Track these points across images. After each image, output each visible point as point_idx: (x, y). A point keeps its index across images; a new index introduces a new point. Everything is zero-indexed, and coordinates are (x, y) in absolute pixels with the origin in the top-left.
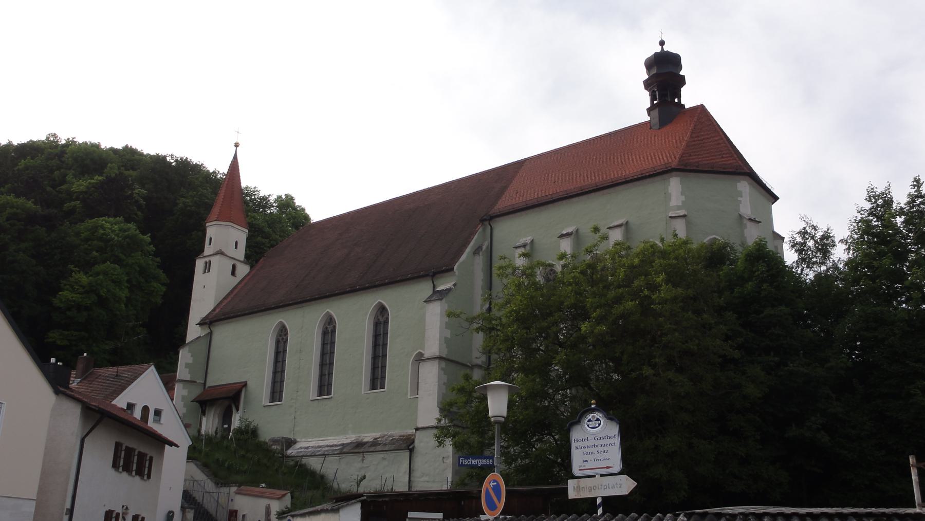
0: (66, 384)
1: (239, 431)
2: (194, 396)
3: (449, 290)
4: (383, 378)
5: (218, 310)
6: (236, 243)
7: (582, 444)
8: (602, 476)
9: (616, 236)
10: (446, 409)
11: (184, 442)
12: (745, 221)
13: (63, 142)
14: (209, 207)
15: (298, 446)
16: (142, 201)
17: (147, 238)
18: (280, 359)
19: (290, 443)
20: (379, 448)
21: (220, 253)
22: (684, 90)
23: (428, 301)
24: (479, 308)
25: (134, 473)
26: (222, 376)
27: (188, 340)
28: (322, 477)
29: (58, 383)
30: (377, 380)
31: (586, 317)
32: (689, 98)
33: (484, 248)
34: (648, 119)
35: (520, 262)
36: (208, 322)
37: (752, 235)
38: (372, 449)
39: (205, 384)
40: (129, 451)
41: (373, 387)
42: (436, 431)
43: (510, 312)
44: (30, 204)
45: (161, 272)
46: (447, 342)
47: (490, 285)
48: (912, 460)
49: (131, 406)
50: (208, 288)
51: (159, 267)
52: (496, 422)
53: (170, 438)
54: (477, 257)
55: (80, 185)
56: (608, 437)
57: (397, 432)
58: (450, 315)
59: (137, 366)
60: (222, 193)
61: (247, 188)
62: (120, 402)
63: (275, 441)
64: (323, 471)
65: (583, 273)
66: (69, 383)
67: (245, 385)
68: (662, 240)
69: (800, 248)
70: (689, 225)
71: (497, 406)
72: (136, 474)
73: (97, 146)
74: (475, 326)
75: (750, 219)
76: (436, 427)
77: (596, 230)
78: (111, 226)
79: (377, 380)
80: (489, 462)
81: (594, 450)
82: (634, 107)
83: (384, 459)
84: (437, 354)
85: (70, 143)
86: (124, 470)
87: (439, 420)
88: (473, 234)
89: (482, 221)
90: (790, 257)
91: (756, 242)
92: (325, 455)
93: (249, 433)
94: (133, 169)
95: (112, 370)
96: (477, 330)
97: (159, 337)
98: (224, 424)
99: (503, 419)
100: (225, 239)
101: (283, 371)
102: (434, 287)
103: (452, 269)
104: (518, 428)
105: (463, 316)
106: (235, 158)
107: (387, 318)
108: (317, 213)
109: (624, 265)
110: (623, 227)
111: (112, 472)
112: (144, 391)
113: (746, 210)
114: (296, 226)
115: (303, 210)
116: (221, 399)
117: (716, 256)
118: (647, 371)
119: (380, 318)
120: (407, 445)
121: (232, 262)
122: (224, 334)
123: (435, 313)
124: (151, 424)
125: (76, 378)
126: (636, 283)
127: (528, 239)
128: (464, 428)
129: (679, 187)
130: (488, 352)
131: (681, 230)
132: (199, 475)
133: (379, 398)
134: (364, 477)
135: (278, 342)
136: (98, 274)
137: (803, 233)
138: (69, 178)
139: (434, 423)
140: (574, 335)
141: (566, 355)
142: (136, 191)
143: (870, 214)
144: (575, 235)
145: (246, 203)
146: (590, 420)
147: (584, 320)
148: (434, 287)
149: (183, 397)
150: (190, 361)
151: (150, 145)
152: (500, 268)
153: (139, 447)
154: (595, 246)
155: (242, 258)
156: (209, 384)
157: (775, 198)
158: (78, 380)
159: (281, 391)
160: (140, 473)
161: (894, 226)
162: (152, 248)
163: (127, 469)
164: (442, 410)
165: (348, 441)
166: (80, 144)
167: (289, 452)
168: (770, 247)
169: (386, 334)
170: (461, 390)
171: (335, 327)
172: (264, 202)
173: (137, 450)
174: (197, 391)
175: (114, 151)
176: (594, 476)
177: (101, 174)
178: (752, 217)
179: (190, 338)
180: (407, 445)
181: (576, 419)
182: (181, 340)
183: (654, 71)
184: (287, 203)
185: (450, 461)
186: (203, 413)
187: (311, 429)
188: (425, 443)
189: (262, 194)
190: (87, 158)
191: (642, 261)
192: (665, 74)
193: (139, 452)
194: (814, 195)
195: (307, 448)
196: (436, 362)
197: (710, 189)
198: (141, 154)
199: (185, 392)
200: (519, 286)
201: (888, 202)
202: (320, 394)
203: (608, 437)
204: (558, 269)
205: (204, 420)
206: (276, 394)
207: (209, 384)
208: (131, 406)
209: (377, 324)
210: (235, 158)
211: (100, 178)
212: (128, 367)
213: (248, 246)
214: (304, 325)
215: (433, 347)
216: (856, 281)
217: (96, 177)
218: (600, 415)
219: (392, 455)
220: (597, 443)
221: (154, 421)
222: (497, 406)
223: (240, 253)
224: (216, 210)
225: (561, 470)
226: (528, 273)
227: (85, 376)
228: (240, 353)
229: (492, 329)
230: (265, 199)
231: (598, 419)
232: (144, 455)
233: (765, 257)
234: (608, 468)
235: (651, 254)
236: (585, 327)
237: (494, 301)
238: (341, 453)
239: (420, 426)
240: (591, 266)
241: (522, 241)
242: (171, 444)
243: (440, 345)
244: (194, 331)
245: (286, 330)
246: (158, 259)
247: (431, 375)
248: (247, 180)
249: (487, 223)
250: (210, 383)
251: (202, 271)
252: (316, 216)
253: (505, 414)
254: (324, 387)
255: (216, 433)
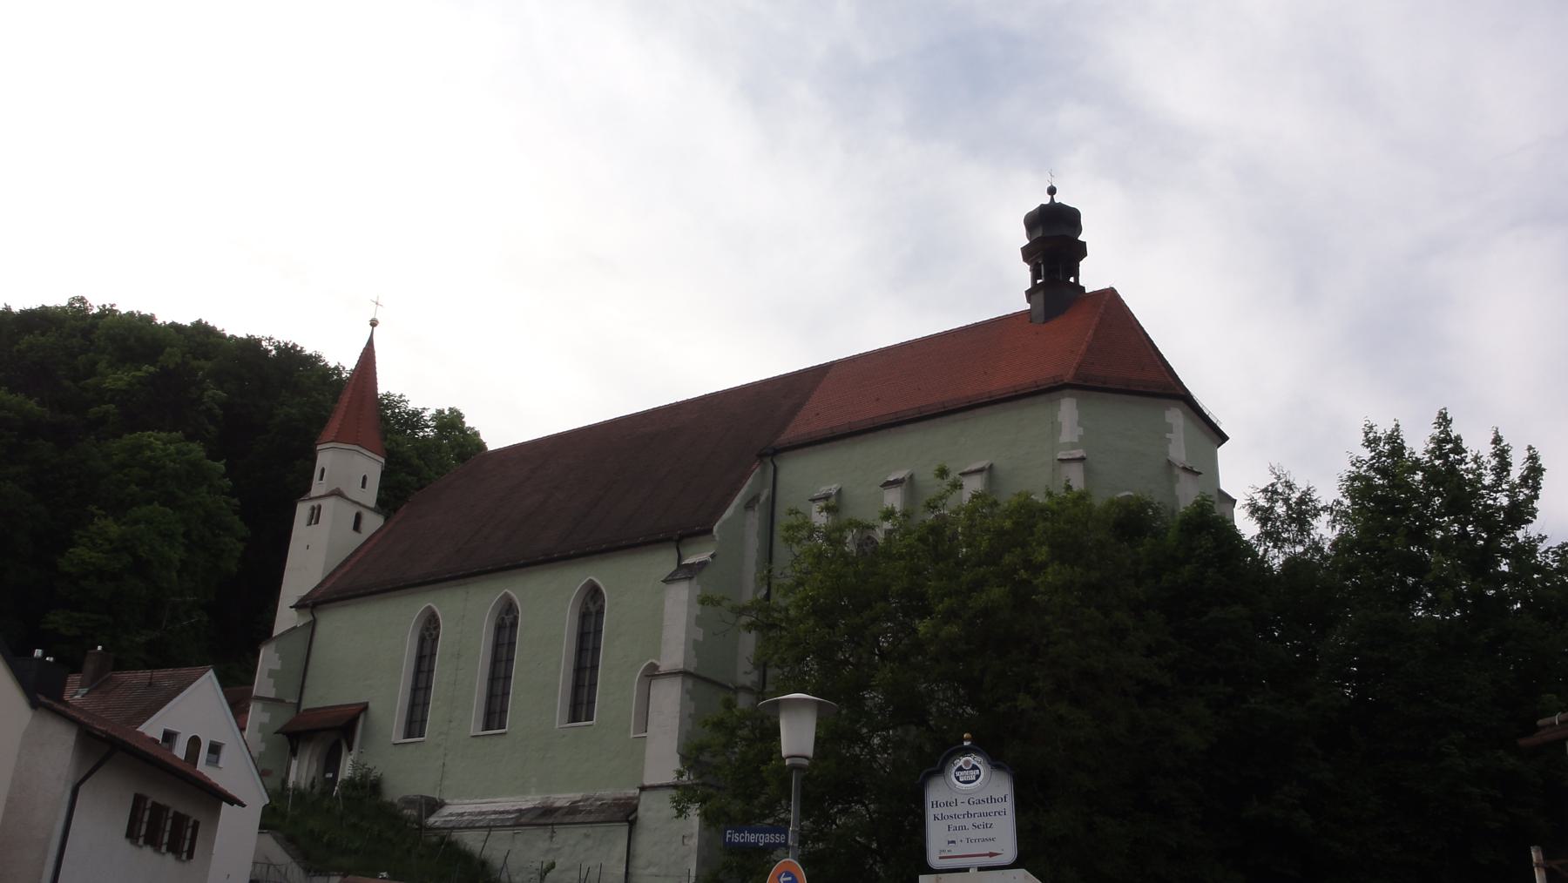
0: (58, 695)
1: (350, 783)
2: (278, 726)
3: (703, 564)
4: (591, 702)
5: (328, 585)
6: (365, 478)
7: (946, 811)
8: (980, 869)
9: (974, 485)
10: (691, 756)
11: (255, 797)
12: (1177, 471)
13: (96, 311)
14: (322, 422)
15: (446, 811)
16: (218, 411)
17: (220, 466)
18: (425, 667)
19: (434, 805)
20: (579, 818)
21: (337, 493)
22: (1084, 265)
23: (670, 580)
24: (750, 592)
25: (164, 849)
26: (328, 691)
27: (275, 633)
28: (484, 864)
29: (42, 692)
30: (581, 705)
31: (925, 612)
32: (1091, 276)
33: (763, 499)
34: (1028, 307)
35: (820, 519)
36: (311, 604)
37: (1187, 495)
38: (567, 820)
39: (299, 704)
40: (158, 810)
41: (574, 717)
42: (674, 792)
43: (804, 599)
44: (32, 405)
45: (237, 518)
46: (696, 647)
47: (769, 554)
48: (1536, 855)
49: (169, 736)
50: (314, 549)
51: (235, 513)
52: (794, 767)
53: (231, 791)
54: (751, 513)
55: (118, 379)
56: (992, 800)
57: (609, 793)
58: (704, 601)
59: (184, 671)
60: (345, 398)
61: (388, 395)
62: (153, 728)
63: (409, 802)
64: (486, 853)
65: (921, 539)
66: (62, 692)
67: (364, 708)
68: (1049, 494)
69: (1262, 515)
70: (1088, 473)
71: (797, 736)
72: (168, 850)
73: (149, 319)
74: (745, 620)
75: (1185, 469)
76: (675, 786)
77: (943, 473)
78: (159, 442)
79: (581, 705)
80: (778, 838)
81: (968, 822)
82: (1008, 288)
83: (587, 836)
84: (681, 667)
85: (107, 314)
86: (146, 843)
87: (680, 774)
88: (745, 477)
89: (761, 456)
90: (1247, 527)
91: (1196, 502)
92: (489, 828)
93: (368, 788)
94: (207, 358)
95: (143, 675)
96: (749, 627)
97: (228, 625)
98: (326, 772)
99: (806, 762)
100: (346, 471)
101: (428, 688)
102: (680, 559)
103: (710, 531)
104: (831, 779)
105: (725, 603)
106: (370, 343)
107: (602, 607)
108: (496, 438)
109: (988, 530)
110: (985, 474)
111: (127, 844)
112: (195, 711)
113: (1178, 453)
114: (463, 458)
115: (477, 434)
116: (324, 729)
117: (1132, 521)
118: (1025, 702)
119: (591, 605)
120: (625, 813)
121: (353, 510)
122: (336, 625)
123: (679, 601)
124: (202, 767)
125: (82, 686)
126: (1007, 558)
127: (833, 488)
128: (719, 788)
129: (1075, 414)
130: (762, 665)
131: (1078, 481)
132: (279, 855)
133: (581, 736)
134: (553, 866)
135: (422, 640)
136: (136, 522)
137: (1271, 493)
138: (102, 366)
139: (671, 778)
140: (906, 641)
141: (892, 672)
142: (210, 393)
143: (1371, 467)
144: (908, 484)
145: (385, 420)
146: (960, 769)
147: (922, 618)
148: (680, 559)
149: (262, 727)
150: (277, 666)
151: (235, 321)
152: (789, 528)
153: (176, 804)
154: (941, 498)
155: (372, 503)
156: (306, 705)
157: (1223, 438)
158: (85, 691)
159: (424, 721)
160: (174, 848)
161: (1407, 487)
162: (227, 483)
163: (152, 840)
164: (684, 758)
165: (530, 805)
166: (121, 316)
167: (432, 820)
168: (1218, 510)
169: (598, 632)
170: (719, 725)
171: (516, 618)
172: (414, 419)
173: (171, 804)
174: (285, 716)
175: (175, 327)
176: (966, 870)
177: (153, 364)
178: (1188, 465)
179: (280, 627)
180: (625, 813)
181: (935, 762)
182: (266, 633)
183: (1039, 233)
184: (450, 423)
185: (694, 842)
186: (294, 753)
187: (466, 782)
188: (655, 810)
189: (411, 406)
190: (132, 337)
191: (1016, 523)
192: (1054, 238)
193: (176, 813)
194: (1282, 433)
195: (462, 814)
196: (678, 681)
197: (1124, 421)
198: (221, 336)
199: (265, 718)
200: (819, 556)
201: (1397, 449)
202: (487, 726)
203: (992, 800)
204: (879, 536)
205: (294, 764)
206: (415, 724)
207: (306, 705)
208: (169, 736)
209: (584, 616)
210: (370, 343)
211: (152, 369)
212: (170, 671)
213: (384, 486)
214: (466, 614)
215: (673, 655)
216: (1351, 571)
217: (145, 367)
218: (979, 759)
219: (601, 830)
220: (973, 809)
221: (208, 762)
222: (797, 736)
223: (370, 496)
224: (334, 425)
225: (875, 862)
226: (834, 536)
227: (97, 683)
228: (361, 656)
229: (772, 626)
230: (416, 414)
231: (975, 767)
232: (185, 818)
233: (1210, 518)
234: (992, 855)
235: (1027, 513)
236: (923, 627)
237: (775, 582)
238: (517, 824)
239: (647, 783)
240: (936, 530)
241: (824, 490)
242: (232, 801)
243: (686, 652)
244: (286, 618)
245: (437, 621)
246: (235, 501)
247: (668, 701)
248: (387, 383)
249: (768, 460)
250: (307, 704)
251: (305, 521)
252: (491, 447)
253: (810, 752)
254: (494, 715)
255: (312, 786)
